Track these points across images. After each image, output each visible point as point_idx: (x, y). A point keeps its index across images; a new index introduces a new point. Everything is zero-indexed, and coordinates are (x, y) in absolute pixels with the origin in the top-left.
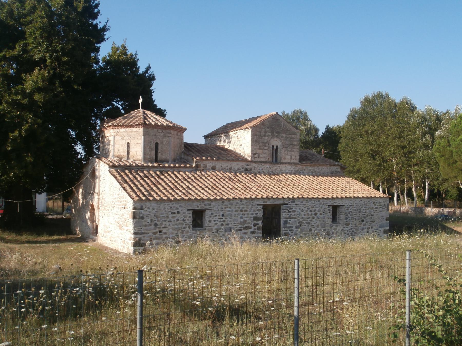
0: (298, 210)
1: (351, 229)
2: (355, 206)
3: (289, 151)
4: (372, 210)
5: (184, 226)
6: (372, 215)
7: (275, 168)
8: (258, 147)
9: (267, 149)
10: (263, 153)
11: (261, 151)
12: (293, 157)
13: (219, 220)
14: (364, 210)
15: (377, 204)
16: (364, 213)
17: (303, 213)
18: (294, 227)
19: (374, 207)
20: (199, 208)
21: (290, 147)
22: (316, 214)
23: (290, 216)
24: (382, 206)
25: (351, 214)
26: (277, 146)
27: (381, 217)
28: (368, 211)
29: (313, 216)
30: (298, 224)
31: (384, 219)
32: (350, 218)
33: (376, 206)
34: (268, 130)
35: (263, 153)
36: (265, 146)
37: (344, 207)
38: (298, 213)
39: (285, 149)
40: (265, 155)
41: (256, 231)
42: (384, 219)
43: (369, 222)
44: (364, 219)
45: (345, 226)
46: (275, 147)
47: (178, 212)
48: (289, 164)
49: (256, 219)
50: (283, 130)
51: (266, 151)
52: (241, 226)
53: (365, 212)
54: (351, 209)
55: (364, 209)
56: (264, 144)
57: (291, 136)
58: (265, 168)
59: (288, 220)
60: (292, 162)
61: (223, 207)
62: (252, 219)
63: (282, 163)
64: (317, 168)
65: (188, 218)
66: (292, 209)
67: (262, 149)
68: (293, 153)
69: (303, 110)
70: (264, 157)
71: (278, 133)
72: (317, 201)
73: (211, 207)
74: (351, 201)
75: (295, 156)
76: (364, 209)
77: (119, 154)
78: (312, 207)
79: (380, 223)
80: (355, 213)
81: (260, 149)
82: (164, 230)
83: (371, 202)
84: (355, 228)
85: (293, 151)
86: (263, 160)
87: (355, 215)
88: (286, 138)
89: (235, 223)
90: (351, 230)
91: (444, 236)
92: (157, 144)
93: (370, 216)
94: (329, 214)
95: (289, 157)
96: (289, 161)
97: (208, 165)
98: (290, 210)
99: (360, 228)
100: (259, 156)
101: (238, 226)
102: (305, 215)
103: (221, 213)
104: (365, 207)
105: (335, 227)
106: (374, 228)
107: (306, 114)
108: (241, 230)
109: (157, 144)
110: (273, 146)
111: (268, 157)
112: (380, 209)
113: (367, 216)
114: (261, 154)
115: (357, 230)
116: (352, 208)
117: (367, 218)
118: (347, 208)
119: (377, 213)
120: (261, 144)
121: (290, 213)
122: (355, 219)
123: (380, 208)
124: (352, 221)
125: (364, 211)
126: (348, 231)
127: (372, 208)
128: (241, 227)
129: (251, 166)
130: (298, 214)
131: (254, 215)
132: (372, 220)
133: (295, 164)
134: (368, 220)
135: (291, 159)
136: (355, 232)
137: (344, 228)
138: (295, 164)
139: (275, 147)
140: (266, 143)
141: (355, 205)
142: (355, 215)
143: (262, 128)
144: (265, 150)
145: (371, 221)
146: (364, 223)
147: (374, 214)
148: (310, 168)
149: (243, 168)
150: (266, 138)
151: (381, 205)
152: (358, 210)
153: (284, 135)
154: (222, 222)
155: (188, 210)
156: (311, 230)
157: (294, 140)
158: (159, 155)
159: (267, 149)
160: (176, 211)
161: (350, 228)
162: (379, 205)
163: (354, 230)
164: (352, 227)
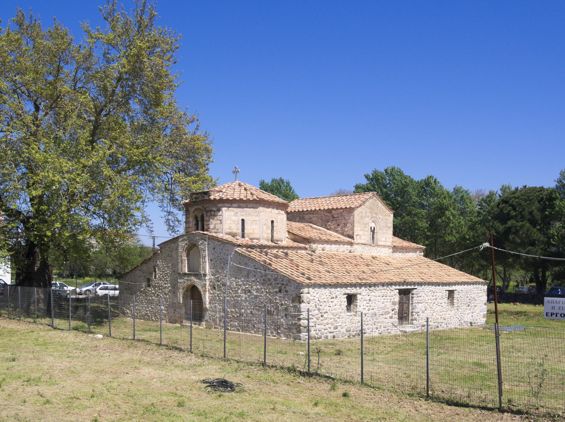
0: (424, 295)
5: (340, 310)
8: (360, 228)
11: (362, 232)
12: (387, 240)
13: (367, 305)
18: (421, 312)
20: (352, 293)
26: (374, 228)
29: (435, 300)
34: (368, 210)
40: (365, 237)
41: (394, 315)
43: (473, 307)
46: (373, 229)
47: (336, 297)
49: (394, 303)
51: (366, 232)
52: (383, 311)
56: (364, 225)
59: (417, 304)
63: (378, 246)
65: (343, 303)
69: (285, 179)
70: (365, 239)
77: (230, 231)
82: (325, 315)
86: (363, 242)
91: (346, 304)
92: (272, 222)
94: (445, 299)
96: (384, 243)
98: (418, 295)
100: (360, 238)
103: (368, 298)
107: (288, 184)
108: (382, 315)
109: (272, 222)
110: (371, 228)
121: (418, 298)
125: (470, 296)
131: (392, 300)
139: (373, 229)
140: (366, 224)
146: (470, 307)
149: (347, 250)
150: (367, 219)
154: (369, 307)
155: (344, 294)
158: (275, 235)
160: (334, 296)
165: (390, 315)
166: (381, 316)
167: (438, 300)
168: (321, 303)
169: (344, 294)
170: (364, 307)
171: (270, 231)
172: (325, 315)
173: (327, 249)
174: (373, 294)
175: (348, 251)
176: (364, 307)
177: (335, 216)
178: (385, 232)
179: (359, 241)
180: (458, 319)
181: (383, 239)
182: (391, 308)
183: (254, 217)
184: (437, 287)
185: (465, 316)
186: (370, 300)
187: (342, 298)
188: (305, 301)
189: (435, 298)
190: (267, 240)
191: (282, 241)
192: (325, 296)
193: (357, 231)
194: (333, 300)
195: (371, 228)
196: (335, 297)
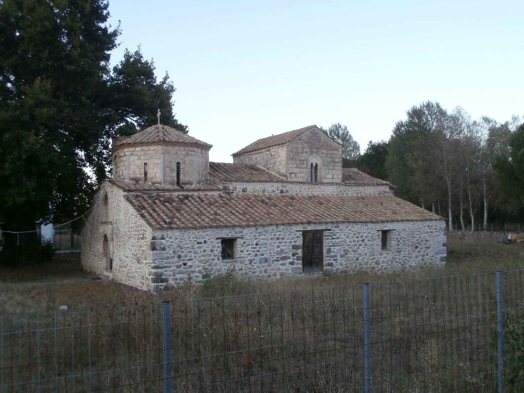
0: (343, 236)
1: (404, 257)
2: (407, 230)
3: (330, 169)
4: (427, 235)
5: (212, 257)
6: (427, 241)
7: (315, 189)
8: (295, 166)
9: (305, 168)
10: (300, 172)
11: (298, 169)
12: (335, 176)
13: (253, 250)
14: (417, 234)
15: (432, 228)
16: (418, 239)
17: (348, 240)
19: (429, 231)
20: (229, 236)
21: (332, 164)
22: (363, 241)
23: (333, 244)
24: (438, 230)
25: (403, 239)
26: (316, 164)
27: (437, 243)
28: (422, 236)
29: (360, 242)
30: (343, 253)
31: (440, 244)
32: (402, 244)
33: (432, 230)
35: (300, 172)
36: (303, 164)
37: (395, 231)
38: (343, 240)
39: (326, 167)
40: (303, 175)
41: (296, 261)
42: (440, 244)
43: (424, 249)
44: (418, 245)
45: (397, 254)
46: (314, 165)
47: (205, 242)
48: (331, 184)
49: (295, 247)
50: (323, 145)
51: (304, 170)
52: (278, 256)
53: (419, 237)
54: (403, 234)
55: (418, 233)
56: (301, 162)
57: (332, 152)
58: (304, 190)
59: (332, 248)
60: (334, 182)
61: (257, 235)
62: (291, 247)
63: (322, 184)
64: (363, 189)
66: (336, 235)
67: (299, 168)
68: (335, 171)
70: (302, 177)
71: (317, 148)
72: (364, 226)
73: (243, 235)
74: (403, 225)
75: (338, 175)
76: (418, 233)
77: (135, 176)
78: (359, 233)
79: (436, 250)
80: (408, 239)
81: (297, 167)
83: (425, 225)
84: (408, 255)
85: (335, 169)
86: (301, 180)
87: (407, 240)
88: (327, 154)
89: (270, 253)
90: (404, 258)
92: (178, 163)
93: (425, 242)
94: (378, 240)
95: (330, 176)
96: (330, 181)
97: (238, 187)
98: (334, 237)
99: (414, 255)
100: (296, 176)
101: (275, 256)
102: (350, 242)
104: (419, 232)
105: (385, 255)
106: (430, 255)
108: (278, 261)
109: (178, 163)
110: (312, 164)
111: (306, 177)
112: (436, 233)
113: (422, 241)
114: (299, 173)
115: (410, 257)
116: (405, 233)
117: (422, 243)
118: (398, 233)
119: (432, 238)
120: (298, 162)
121: (333, 240)
122: (408, 245)
123: (436, 232)
124: (405, 247)
125: (418, 236)
126: (400, 259)
127: (427, 233)
128: (278, 257)
129: (287, 188)
130: (343, 241)
131: (293, 243)
132: (427, 246)
133: (337, 184)
134: (423, 246)
135: (333, 178)
136: (408, 261)
137: (396, 255)
138: (337, 184)
139: (314, 165)
140: (303, 161)
141: (407, 229)
142: (407, 240)
143: (299, 144)
144: (303, 168)
145: (426, 248)
146: (418, 249)
147: (430, 239)
148: (355, 189)
149: (278, 190)
150: (304, 155)
151: (437, 229)
152: (411, 235)
153: (324, 151)
154: (256, 252)
155: (217, 239)
156: (357, 259)
157: (336, 156)
158: (181, 176)
159: (305, 168)
160: (202, 241)
161: (402, 256)
162: (435, 229)
163: (407, 258)
164: (404, 254)
165: (291, 260)
166: (275, 262)
167: (366, 241)
168: (183, 250)
169: (217, 239)
170: (249, 252)
171: (175, 174)
172: (189, 263)
173: (249, 189)
174: (262, 237)
175: (279, 191)
176: (248, 253)
177: (273, 154)
178: (331, 168)
179: (294, 179)
180: (400, 263)
181: (330, 176)
182: (291, 253)
183: (155, 160)
184: (434, 222)
185: (411, 260)
186: (257, 244)
187: (215, 243)
188: (158, 248)
189: (360, 239)
190: (172, 184)
191: (191, 184)
192: (188, 241)
193: (291, 169)
194: (200, 245)
195: (312, 164)
196: (203, 242)
